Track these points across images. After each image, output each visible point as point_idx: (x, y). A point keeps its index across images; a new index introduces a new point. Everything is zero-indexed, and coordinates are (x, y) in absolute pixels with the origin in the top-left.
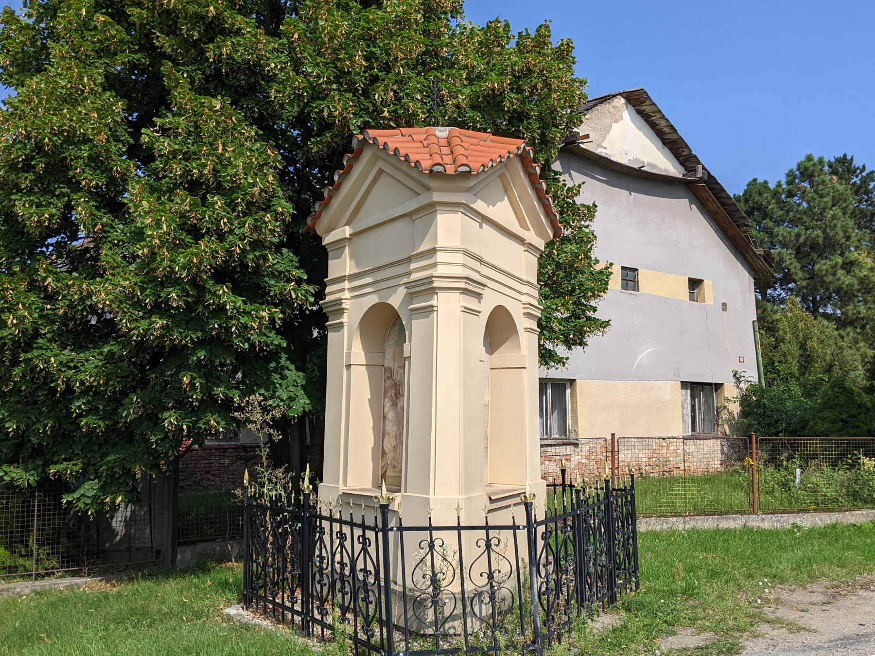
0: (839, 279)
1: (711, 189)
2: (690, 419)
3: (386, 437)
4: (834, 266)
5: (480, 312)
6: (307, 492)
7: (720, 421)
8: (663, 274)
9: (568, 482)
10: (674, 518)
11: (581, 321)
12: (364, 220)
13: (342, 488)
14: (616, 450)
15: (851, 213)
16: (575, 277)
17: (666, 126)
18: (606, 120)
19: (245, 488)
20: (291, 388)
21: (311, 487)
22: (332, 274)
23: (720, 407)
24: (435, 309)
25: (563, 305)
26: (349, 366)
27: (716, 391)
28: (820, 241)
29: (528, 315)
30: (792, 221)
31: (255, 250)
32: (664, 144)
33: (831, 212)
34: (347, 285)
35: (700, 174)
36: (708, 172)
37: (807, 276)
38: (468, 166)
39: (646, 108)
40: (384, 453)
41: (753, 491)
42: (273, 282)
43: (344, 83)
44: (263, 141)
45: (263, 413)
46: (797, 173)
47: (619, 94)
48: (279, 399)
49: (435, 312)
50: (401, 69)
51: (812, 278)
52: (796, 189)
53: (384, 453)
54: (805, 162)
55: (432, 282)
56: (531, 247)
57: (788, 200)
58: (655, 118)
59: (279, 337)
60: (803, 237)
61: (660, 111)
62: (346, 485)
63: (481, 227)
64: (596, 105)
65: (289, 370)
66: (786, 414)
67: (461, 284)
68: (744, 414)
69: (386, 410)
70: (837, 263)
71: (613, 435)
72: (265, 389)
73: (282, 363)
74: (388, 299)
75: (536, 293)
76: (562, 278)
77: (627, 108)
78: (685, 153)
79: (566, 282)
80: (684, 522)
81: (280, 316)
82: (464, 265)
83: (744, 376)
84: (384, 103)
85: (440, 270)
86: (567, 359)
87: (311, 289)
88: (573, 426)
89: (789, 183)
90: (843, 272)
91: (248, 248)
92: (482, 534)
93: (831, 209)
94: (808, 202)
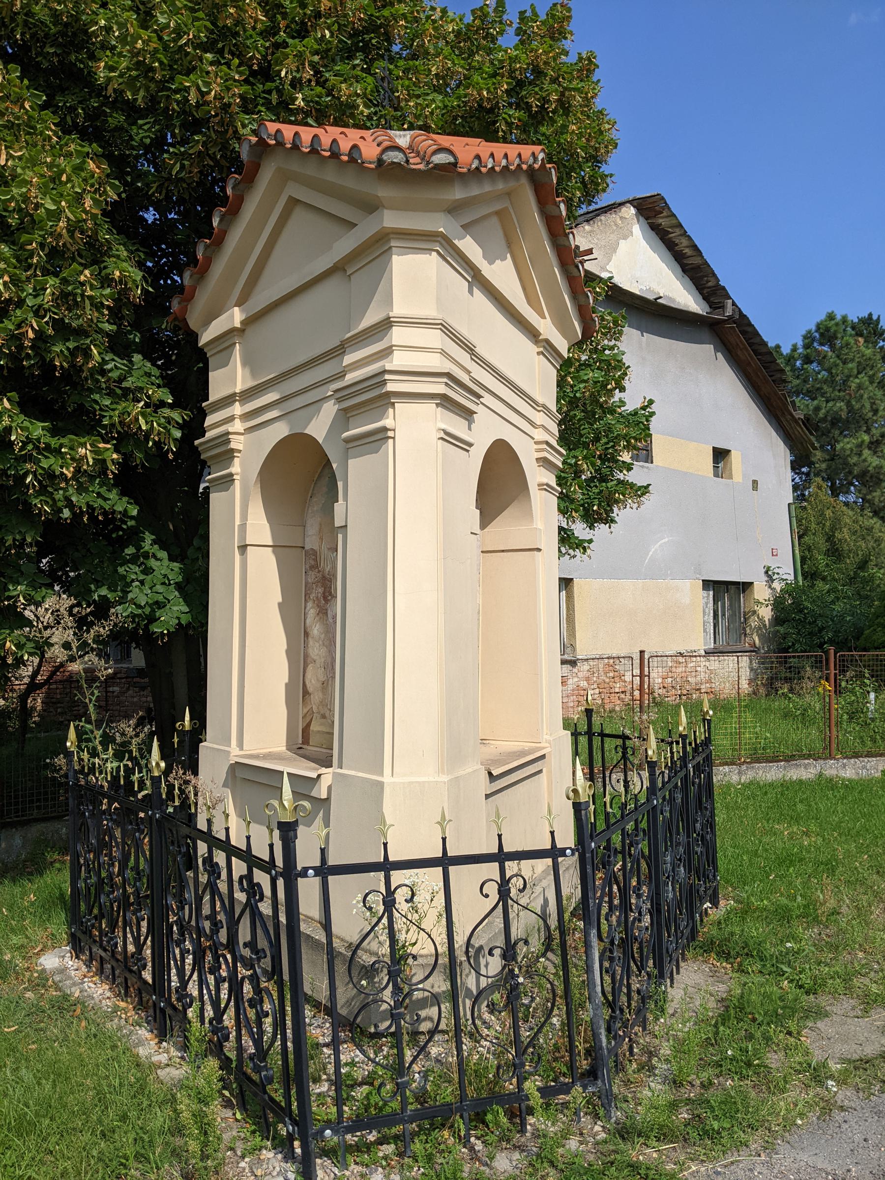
0: (865, 460)
1: (744, 333)
2: (712, 628)
3: (310, 668)
4: (860, 445)
5: (471, 445)
6: (156, 774)
7: (748, 631)
8: (682, 441)
9: (596, 729)
10: (726, 767)
11: (610, 484)
12: (262, 298)
13: (235, 754)
14: (646, 673)
15: (879, 383)
16: (600, 418)
17: (687, 247)
18: (612, 235)
19: (68, 755)
20: (159, 588)
21: (163, 765)
22: (215, 393)
23: (749, 612)
24: (390, 434)
25: (585, 458)
26: (243, 548)
27: (744, 592)
28: (844, 415)
29: (545, 462)
30: (810, 392)
31: (69, 340)
32: (684, 271)
33: (857, 381)
34: (237, 409)
35: (729, 312)
36: (740, 309)
37: (827, 457)
38: (450, 152)
39: (663, 221)
40: (306, 693)
41: (829, 726)
42: (107, 402)
43: (226, 51)
44: (36, 89)
45: (79, 628)
46: (817, 335)
47: (629, 202)
48: (135, 604)
49: (391, 441)
50: (327, 32)
51: (832, 459)
52: (814, 354)
53: (306, 693)
54: (826, 321)
55: (384, 383)
56: (548, 348)
57: (805, 366)
58: (674, 235)
59: (125, 499)
60: (823, 411)
61: (680, 225)
62: (241, 749)
63: (471, 292)
64: (598, 215)
65: (157, 559)
66: (833, 621)
67: (438, 387)
68: (778, 620)
69: (308, 621)
70: (863, 442)
71: (642, 652)
72: (109, 589)
73: (146, 548)
74: (306, 427)
75: (555, 429)
76: (580, 420)
77: (638, 221)
78: (710, 284)
79: (586, 426)
80: (739, 773)
81: (115, 456)
82: (443, 353)
83: (778, 574)
84: (296, 84)
85: (399, 360)
86: (590, 541)
87: (176, 416)
88: (569, 639)
89: (806, 346)
90: (869, 452)
91: (50, 332)
92: (491, 870)
93: (856, 377)
94: (829, 371)
